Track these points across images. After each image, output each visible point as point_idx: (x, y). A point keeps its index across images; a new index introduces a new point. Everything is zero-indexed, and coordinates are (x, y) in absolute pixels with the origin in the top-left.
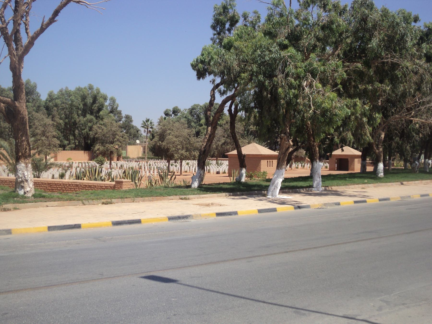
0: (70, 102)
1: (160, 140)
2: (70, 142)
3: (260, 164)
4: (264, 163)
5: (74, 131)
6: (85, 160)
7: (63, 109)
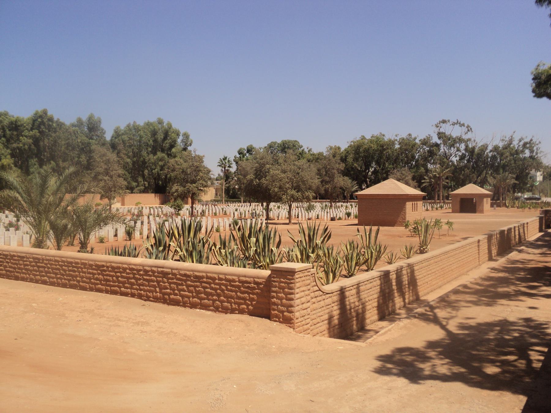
0: (138, 138)
1: (256, 178)
2: (138, 184)
3: (405, 208)
4: (409, 205)
5: (143, 172)
6: (155, 204)
7: (130, 146)
